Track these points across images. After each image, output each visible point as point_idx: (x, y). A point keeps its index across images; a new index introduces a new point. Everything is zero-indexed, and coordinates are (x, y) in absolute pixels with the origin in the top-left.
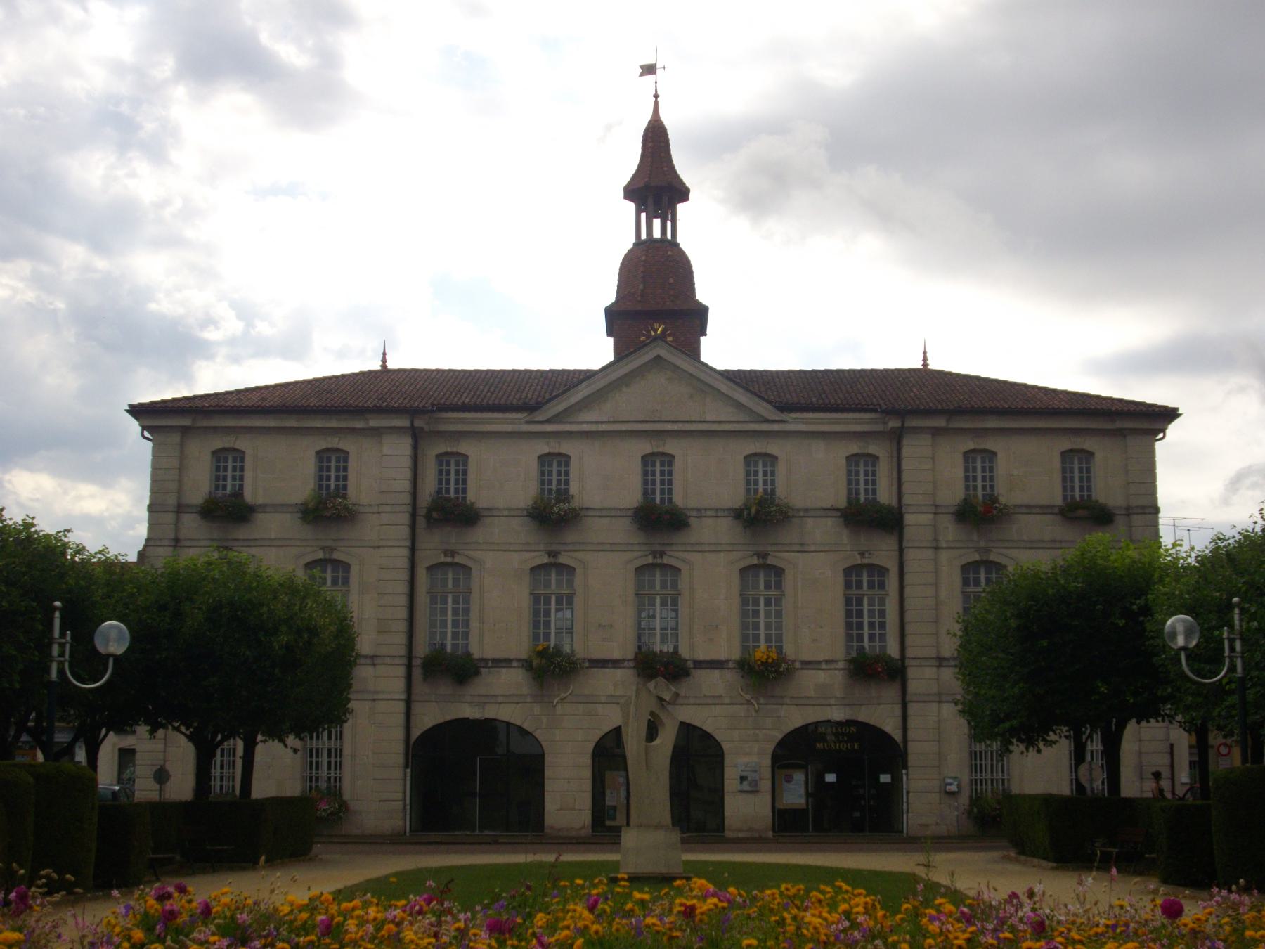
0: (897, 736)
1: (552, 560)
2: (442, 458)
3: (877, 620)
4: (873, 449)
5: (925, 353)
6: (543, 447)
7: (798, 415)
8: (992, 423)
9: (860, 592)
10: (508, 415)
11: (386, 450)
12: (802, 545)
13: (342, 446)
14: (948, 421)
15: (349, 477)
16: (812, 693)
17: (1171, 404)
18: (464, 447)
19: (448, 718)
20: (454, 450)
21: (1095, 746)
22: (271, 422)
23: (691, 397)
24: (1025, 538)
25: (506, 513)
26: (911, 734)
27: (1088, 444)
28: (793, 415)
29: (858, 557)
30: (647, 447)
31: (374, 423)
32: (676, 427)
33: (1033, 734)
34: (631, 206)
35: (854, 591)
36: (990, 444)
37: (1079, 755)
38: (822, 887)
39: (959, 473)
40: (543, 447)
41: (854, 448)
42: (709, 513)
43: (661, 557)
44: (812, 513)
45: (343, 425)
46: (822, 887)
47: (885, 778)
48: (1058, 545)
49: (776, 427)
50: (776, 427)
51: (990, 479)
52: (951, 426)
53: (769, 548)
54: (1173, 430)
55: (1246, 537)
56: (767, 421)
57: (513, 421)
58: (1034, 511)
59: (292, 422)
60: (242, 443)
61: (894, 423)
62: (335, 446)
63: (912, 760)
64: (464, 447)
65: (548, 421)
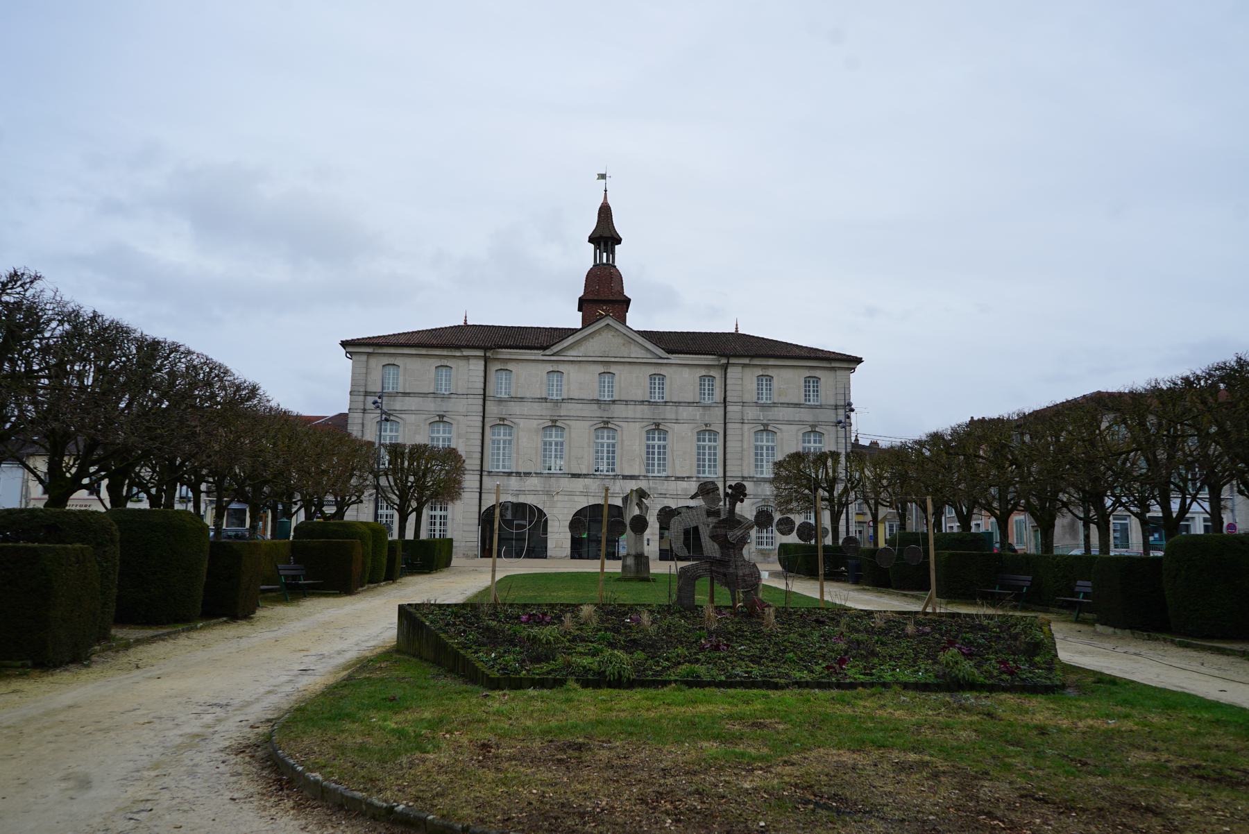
4: (712, 373)
8: (772, 362)
11: (471, 367)
18: (510, 366)
22: (413, 351)
27: (818, 373)
31: (834, 365)
34: (592, 246)
59: (424, 352)
61: (724, 361)
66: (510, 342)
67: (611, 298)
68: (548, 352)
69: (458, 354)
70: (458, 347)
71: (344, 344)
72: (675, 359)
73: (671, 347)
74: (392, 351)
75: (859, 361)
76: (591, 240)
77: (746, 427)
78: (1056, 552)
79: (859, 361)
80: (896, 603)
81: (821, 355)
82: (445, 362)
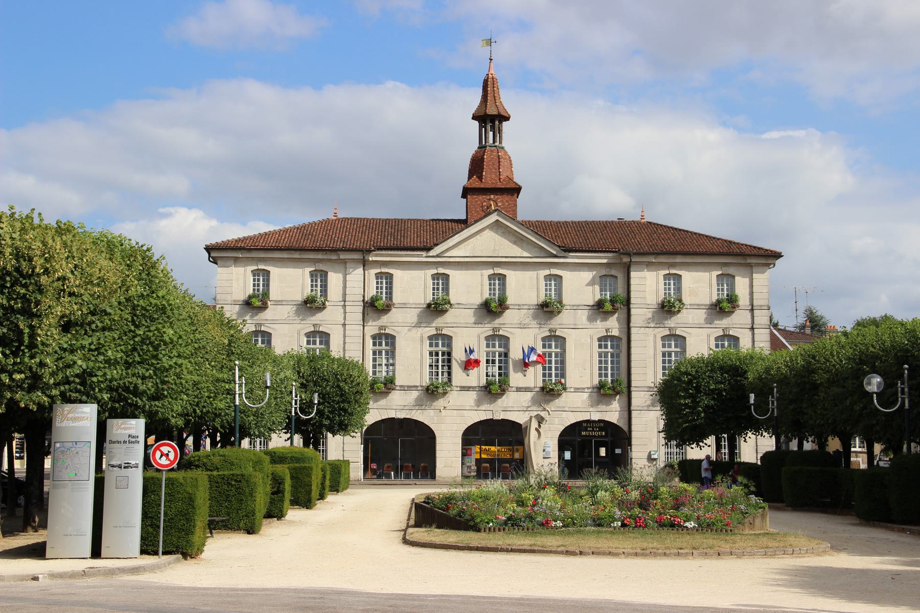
0: (625, 428)
4: (613, 272)
8: (679, 259)
16: (580, 405)
17: (778, 250)
19: (384, 418)
21: (725, 443)
22: (285, 255)
26: (633, 428)
27: (731, 270)
31: (343, 256)
32: (507, 260)
33: (697, 437)
34: (476, 123)
37: (718, 447)
38: (161, 210)
46: (161, 210)
47: (618, 451)
51: (679, 289)
54: (778, 262)
55: (791, 369)
56: (555, 256)
57: (418, 256)
59: (296, 255)
61: (626, 259)
63: (634, 441)
65: (438, 256)
66: (392, 242)
67: (499, 185)
68: (431, 253)
69: (334, 257)
70: (335, 250)
71: (209, 249)
72: (574, 258)
73: (569, 243)
74: (262, 255)
75: (778, 256)
76: (475, 118)
78: (830, 438)
79: (778, 256)
80: (155, 580)
81: (709, 246)
82: (555, 271)
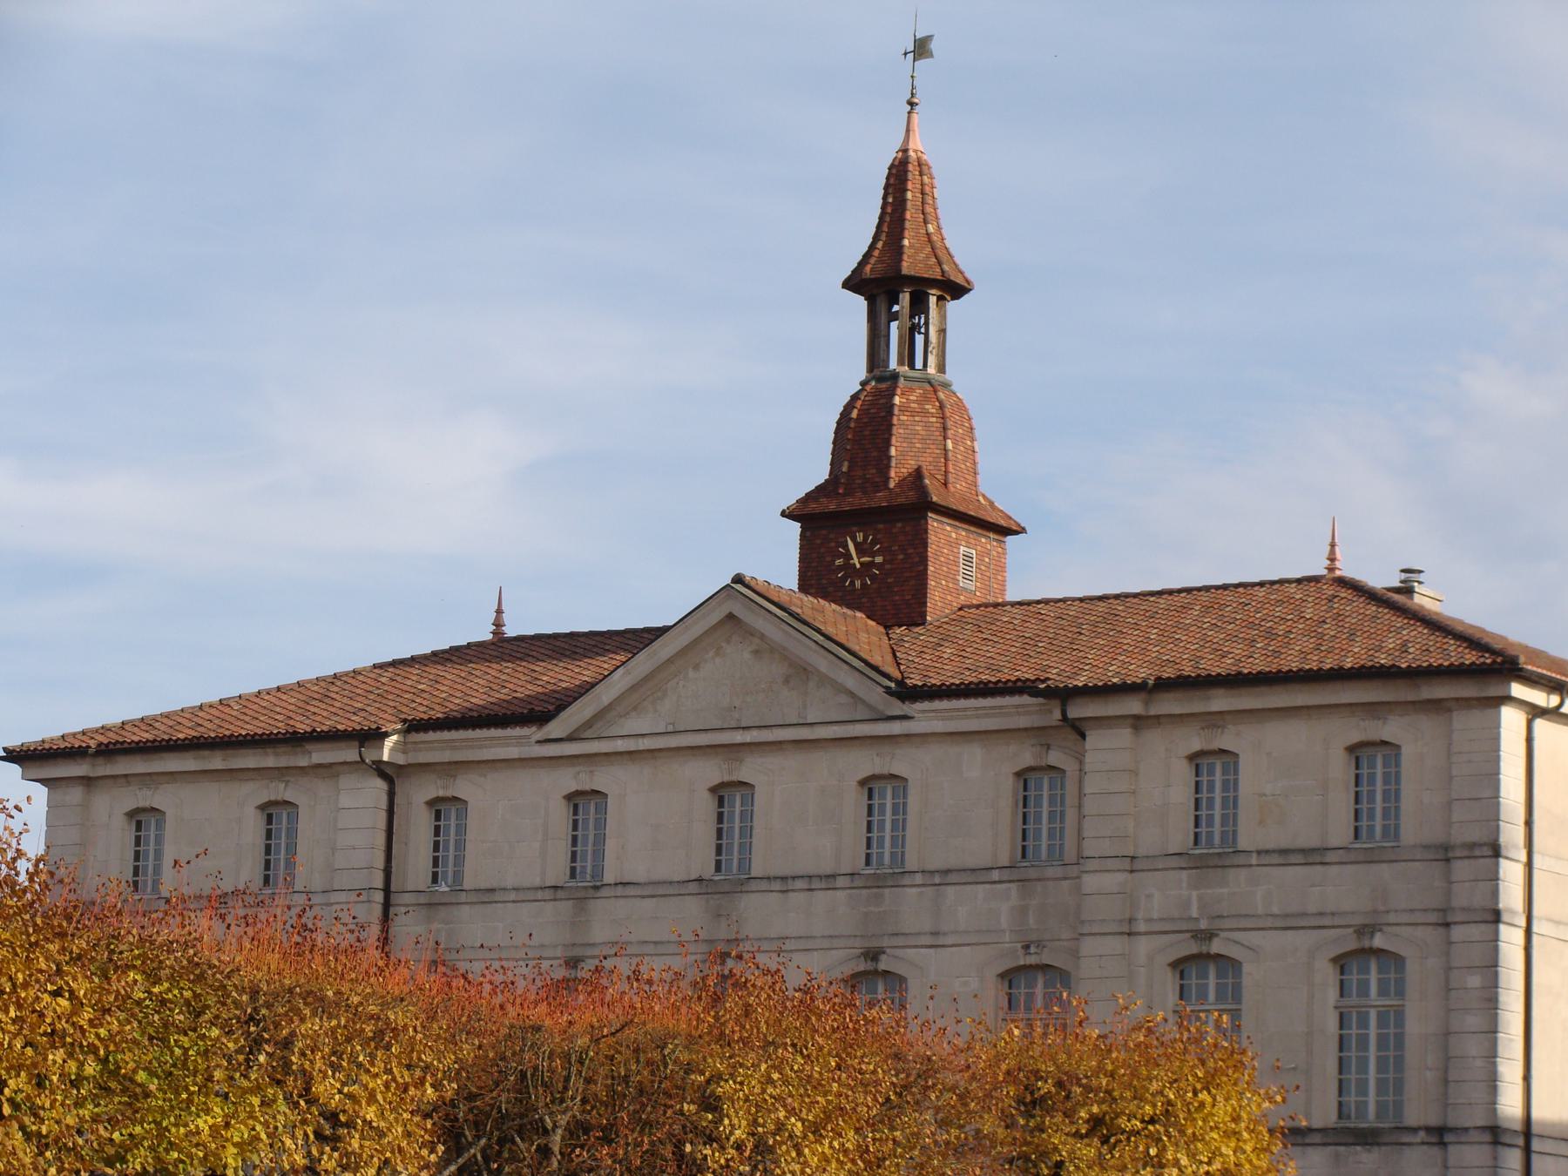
1: (870, 966)
2: (437, 806)
3: (1353, 1054)
5: (499, 612)
6: (569, 780)
7: (926, 705)
9: (1363, 1001)
10: (509, 732)
11: (345, 800)
12: (935, 934)
13: (897, 768)
14: (1147, 704)
15: (1403, 794)
18: (462, 787)
20: (449, 793)
23: (787, 681)
24: (1275, 910)
25: (513, 896)
28: (919, 706)
29: (1021, 952)
30: (711, 772)
35: (1354, 1000)
36: (1226, 740)
39: (1181, 794)
40: (569, 780)
41: (1027, 758)
42: (799, 884)
43: (1372, 935)
44: (952, 878)
45: (283, 762)
48: (1326, 921)
49: (896, 728)
50: (896, 728)
52: (1152, 712)
53: (885, 942)
57: (520, 741)
58: (1293, 859)
59: (216, 761)
60: (158, 798)
62: (147, 804)
64: (462, 787)
65: (570, 738)
77: (1143, 946)
